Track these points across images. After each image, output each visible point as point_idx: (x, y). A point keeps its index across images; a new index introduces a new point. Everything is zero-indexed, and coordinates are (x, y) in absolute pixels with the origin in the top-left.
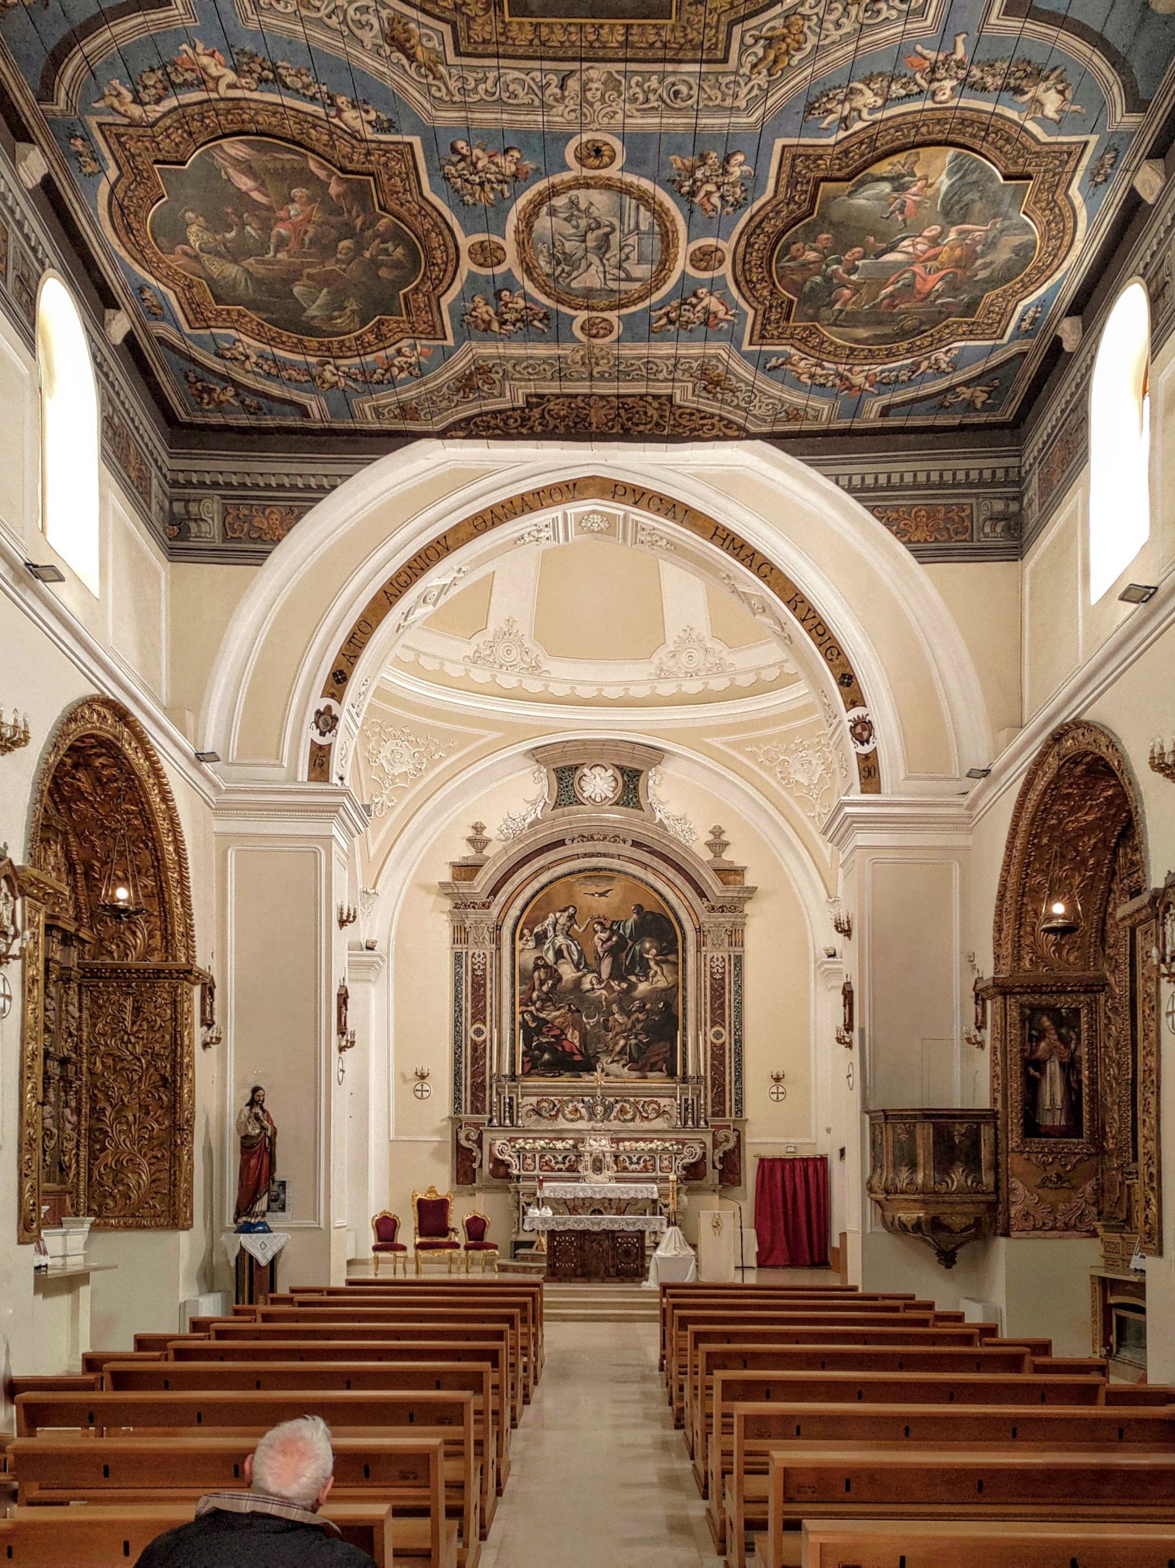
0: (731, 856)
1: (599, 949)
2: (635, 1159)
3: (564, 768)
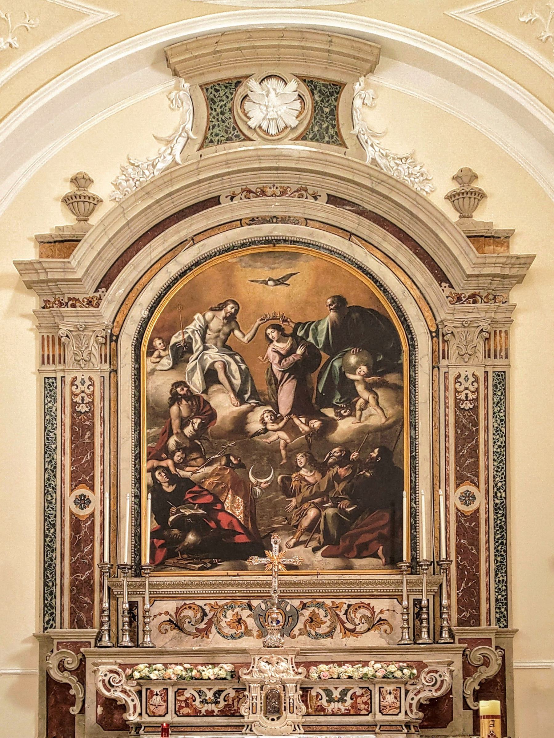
0: (487, 216)
1: (275, 368)
2: (336, 694)
3: (218, 83)
